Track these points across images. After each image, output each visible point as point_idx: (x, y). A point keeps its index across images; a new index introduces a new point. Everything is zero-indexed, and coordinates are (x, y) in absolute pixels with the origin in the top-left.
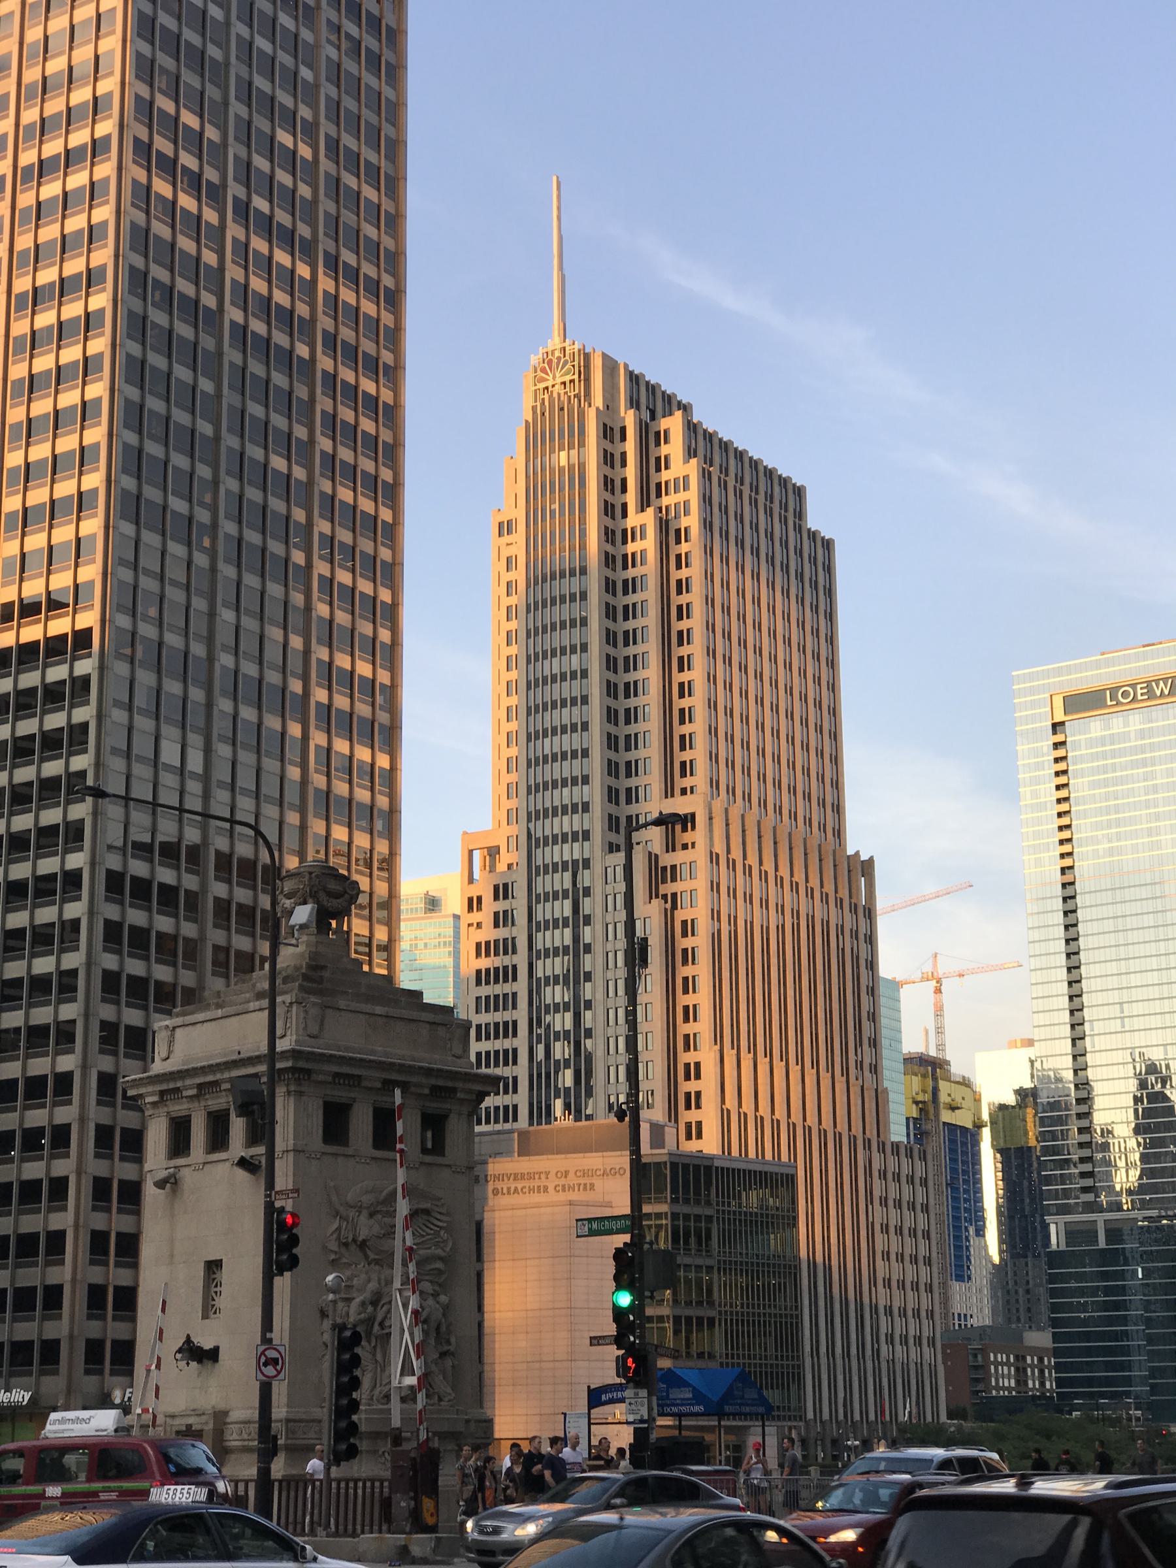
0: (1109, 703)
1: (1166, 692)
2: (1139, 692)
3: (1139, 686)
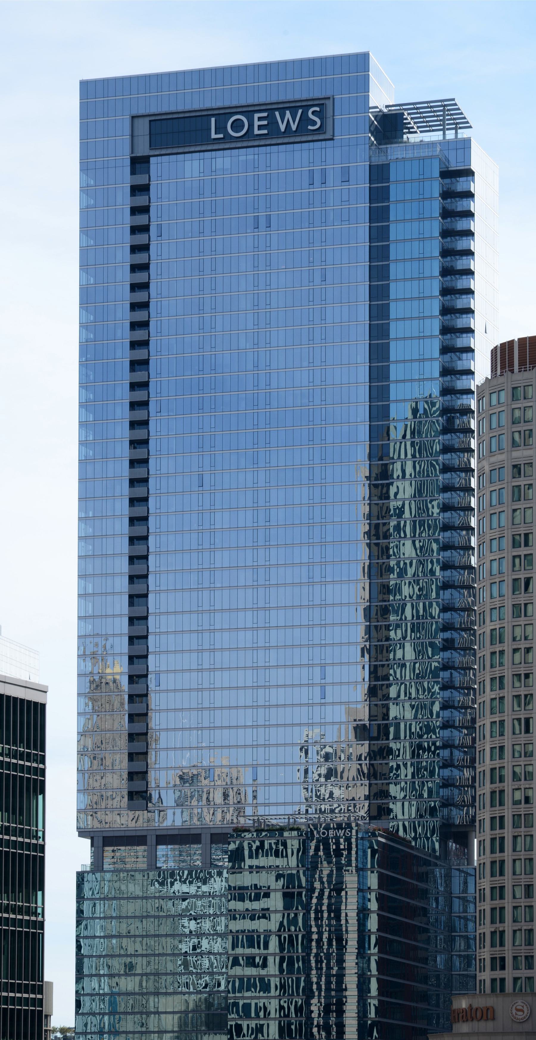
0: (214, 136)
1: (294, 127)
2: (257, 123)
3: (257, 116)
